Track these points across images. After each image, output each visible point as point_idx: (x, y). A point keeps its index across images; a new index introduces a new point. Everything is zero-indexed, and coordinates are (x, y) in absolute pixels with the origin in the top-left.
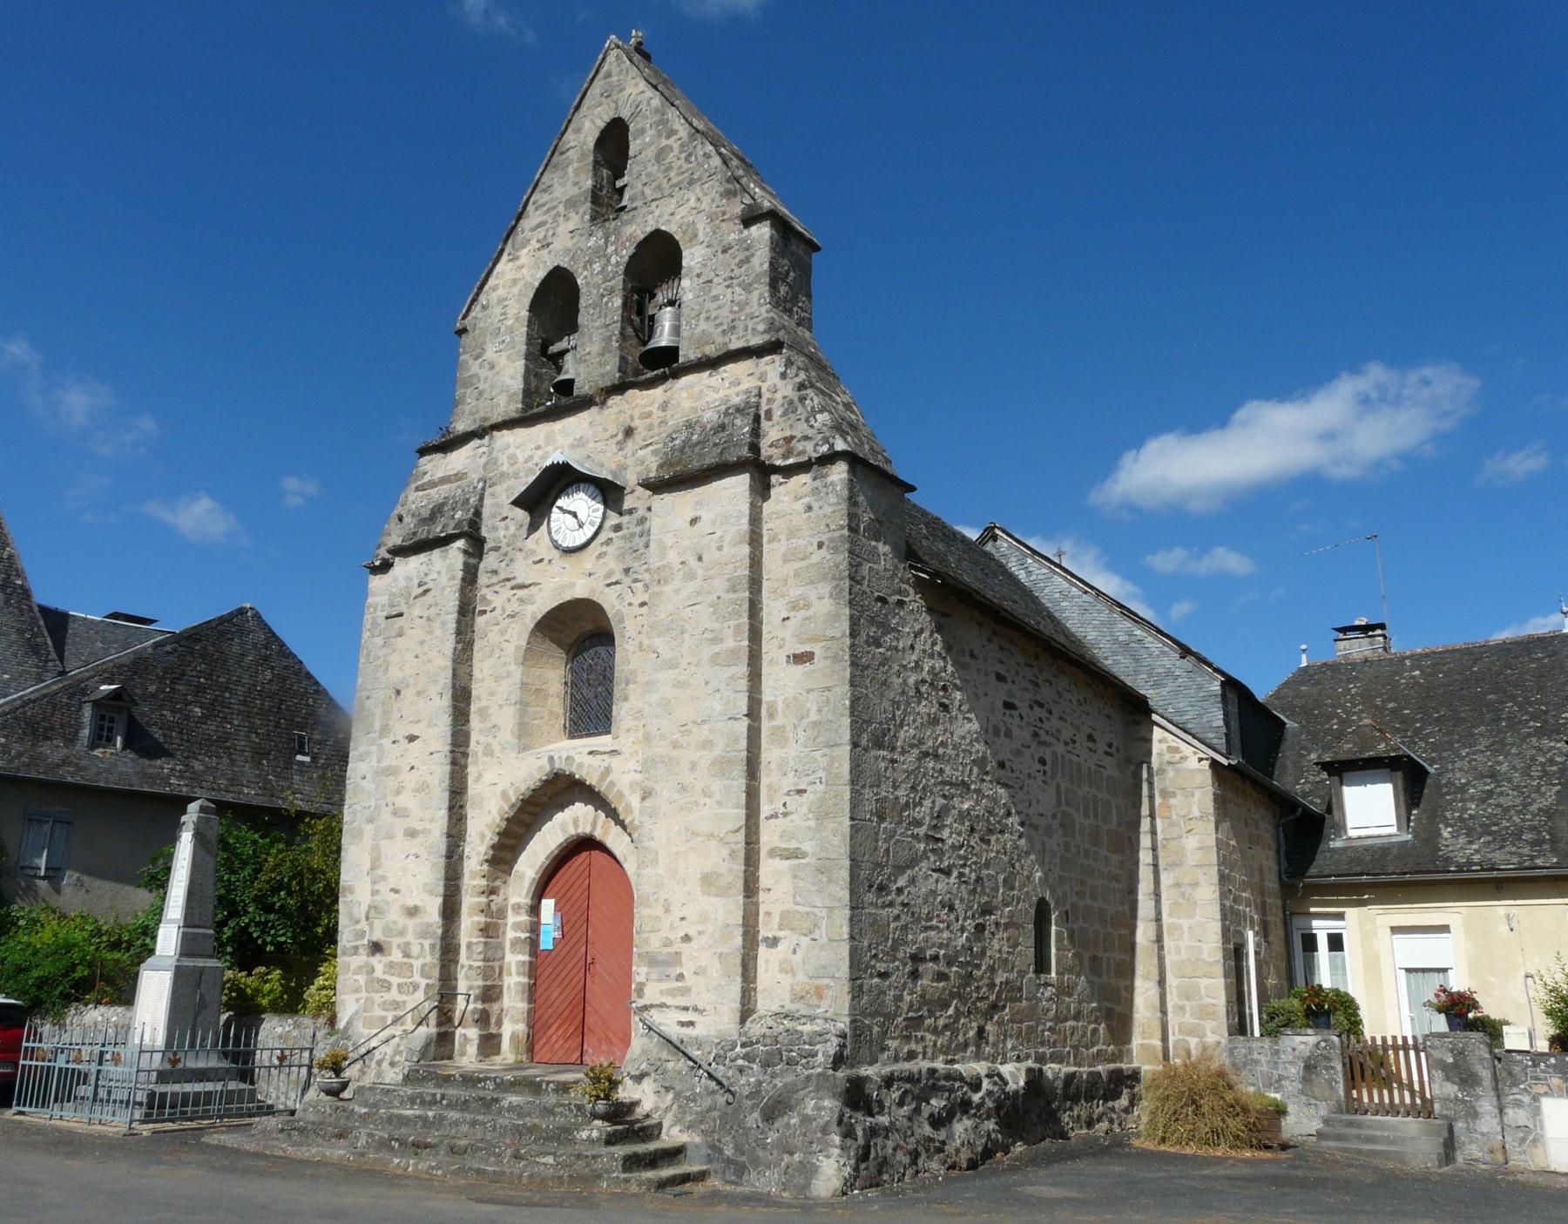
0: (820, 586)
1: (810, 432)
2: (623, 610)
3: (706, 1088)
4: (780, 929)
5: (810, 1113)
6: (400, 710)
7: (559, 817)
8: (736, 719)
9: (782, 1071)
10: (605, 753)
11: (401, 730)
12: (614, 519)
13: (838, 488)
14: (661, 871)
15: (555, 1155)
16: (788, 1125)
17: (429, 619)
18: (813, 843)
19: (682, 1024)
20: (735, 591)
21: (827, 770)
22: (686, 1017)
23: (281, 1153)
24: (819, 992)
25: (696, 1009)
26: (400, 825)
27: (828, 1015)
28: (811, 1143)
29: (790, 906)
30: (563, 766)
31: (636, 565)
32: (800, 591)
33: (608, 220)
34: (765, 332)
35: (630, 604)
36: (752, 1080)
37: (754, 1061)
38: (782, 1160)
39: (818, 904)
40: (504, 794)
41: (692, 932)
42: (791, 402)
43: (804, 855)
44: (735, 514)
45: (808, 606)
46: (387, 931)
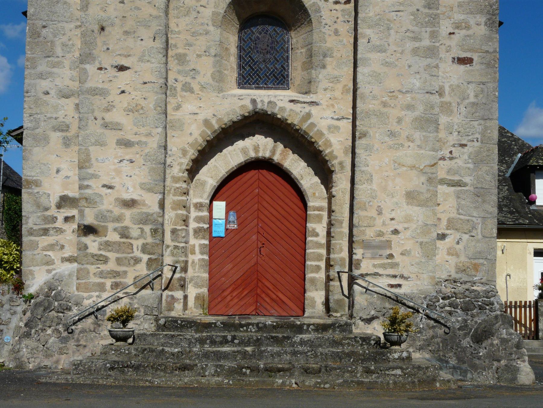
0: (478, 16)
3: (428, 325)
4: (447, 229)
5: (506, 337)
6: (105, 43)
7: (240, 144)
8: (432, 93)
9: (478, 314)
10: (304, 103)
11: (107, 61)
14: (374, 186)
15: (401, 368)
16: (492, 345)
18: (472, 178)
19: (392, 286)
20: (430, 8)
21: (483, 134)
25: (402, 277)
26: (111, 137)
28: (511, 354)
29: (454, 215)
30: (265, 107)
32: (462, 17)
36: (460, 319)
37: (457, 308)
38: (493, 365)
40: (207, 122)
41: (399, 228)
45: (468, 28)
46: (101, 216)
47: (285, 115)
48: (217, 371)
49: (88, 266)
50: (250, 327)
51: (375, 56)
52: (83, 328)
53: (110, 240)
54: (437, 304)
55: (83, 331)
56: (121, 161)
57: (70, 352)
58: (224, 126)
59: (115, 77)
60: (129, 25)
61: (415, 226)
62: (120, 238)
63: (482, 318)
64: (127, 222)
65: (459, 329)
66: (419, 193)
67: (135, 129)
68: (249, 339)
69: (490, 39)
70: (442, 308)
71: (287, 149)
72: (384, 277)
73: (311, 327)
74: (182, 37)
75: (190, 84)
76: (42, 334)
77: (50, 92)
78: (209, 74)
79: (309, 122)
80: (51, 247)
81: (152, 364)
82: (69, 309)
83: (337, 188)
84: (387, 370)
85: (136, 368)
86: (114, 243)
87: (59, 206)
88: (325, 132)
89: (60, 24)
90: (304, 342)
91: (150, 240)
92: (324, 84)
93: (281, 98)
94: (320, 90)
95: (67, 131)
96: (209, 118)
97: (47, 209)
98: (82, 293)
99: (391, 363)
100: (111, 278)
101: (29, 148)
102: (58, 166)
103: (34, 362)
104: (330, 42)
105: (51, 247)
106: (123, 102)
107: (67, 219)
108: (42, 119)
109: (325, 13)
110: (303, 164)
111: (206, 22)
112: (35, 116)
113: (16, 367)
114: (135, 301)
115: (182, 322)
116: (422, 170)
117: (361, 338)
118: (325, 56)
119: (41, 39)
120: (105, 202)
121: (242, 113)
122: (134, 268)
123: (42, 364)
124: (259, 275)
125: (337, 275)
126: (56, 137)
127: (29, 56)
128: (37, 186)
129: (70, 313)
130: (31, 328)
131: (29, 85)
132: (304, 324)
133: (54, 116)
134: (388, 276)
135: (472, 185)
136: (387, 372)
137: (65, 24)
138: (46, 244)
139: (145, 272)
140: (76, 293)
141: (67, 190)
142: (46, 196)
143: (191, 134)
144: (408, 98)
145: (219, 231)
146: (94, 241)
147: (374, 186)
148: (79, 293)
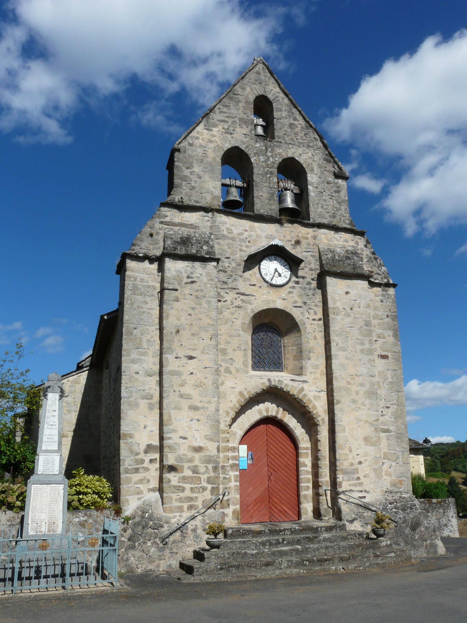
0: (389, 331)
1: (380, 272)
2: (305, 320)
6: (179, 341)
8: (373, 376)
10: (299, 381)
11: (182, 353)
12: (294, 279)
13: (392, 297)
14: (347, 434)
16: (421, 531)
17: (197, 297)
18: (394, 427)
19: (360, 498)
20: (367, 326)
22: (361, 495)
23: (253, 578)
24: (401, 482)
26: (185, 404)
27: (405, 491)
31: (308, 302)
32: (380, 331)
33: (267, 140)
34: (349, 224)
35: (308, 318)
36: (402, 516)
38: (423, 544)
39: (398, 450)
40: (241, 394)
41: (362, 460)
42: (370, 258)
43: (391, 431)
44: (364, 295)
45: (384, 338)
46: (179, 459)
47: (289, 389)
48: (288, 564)
49: (172, 495)
50: (286, 531)
51: (341, 353)
52: (174, 540)
53: (186, 475)
54: (388, 508)
55: (174, 542)
56: (192, 420)
57: (167, 558)
58: (251, 396)
59: (186, 363)
60: (195, 329)
61: (370, 458)
62: (193, 473)
63: (413, 515)
64: (197, 463)
65: (403, 523)
66: (371, 438)
67: (200, 399)
68: (293, 540)
69: (396, 345)
70: (391, 510)
71: (285, 411)
72: (356, 492)
73: (323, 528)
74: (223, 337)
75: (229, 368)
76: (144, 546)
77: (140, 372)
78: (241, 362)
79: (303, 393)
80: (141, 481)
81: (247, 563)
82: (162, 526)
83: (321, 436)
84: (387, 554)
85: (237, 567)
86: (189, 477)
87: (146, 452)
88: (313, 400)
89: (145, 327)
90: (326, 539)
91: (212, 474)
92: (310, 369)
93: (286, 378)
94: (308, 373)
95: (151, 399)
96: (242, 391)
97: (137, 454)
98: (168, 514)
99: (382, 549)
100: (187, 502)
101: (125, 411)
102: (145, 424)
103: (142, 567)
104: (312, 343)
105: (141, 481)
106: (191, 380)
107: (151, 461)
108: (134, 391)
109: (308, 326)
110: (295, 421)
111: (238, 328)
112: (130, 389)
113: (128, 572)
114: (206, 518)
115: (243, 531)
116: (371, 423)
117: (358, 534)
118: (310, 352)
119: (133, 336)
120: (182, 448)
121: (262, 388)
122: (203, 494)
123: (148, 569)
124: (270, 494)
125: (324, 492)
126: (143, 403)
127: (125, 347)
128: (131, 438)
129: (163, 529)
130: (134, 542)
131: (125, 367)
132: (319, 527)
133: (142, 389)
134: (358, 491)
135: (395, 431)
136: (387, 556)
137: (148, 327)
138: (137, 479)
139: (210, 497)
140: (164, 514)
141: (151, 440)
142: (137, 445)
143: (231, 401)
144: (360, 379)
145: (244, 465)
146: (175, 477)
147: (347, 434)
148: (166, 514)
